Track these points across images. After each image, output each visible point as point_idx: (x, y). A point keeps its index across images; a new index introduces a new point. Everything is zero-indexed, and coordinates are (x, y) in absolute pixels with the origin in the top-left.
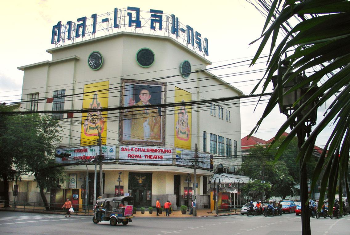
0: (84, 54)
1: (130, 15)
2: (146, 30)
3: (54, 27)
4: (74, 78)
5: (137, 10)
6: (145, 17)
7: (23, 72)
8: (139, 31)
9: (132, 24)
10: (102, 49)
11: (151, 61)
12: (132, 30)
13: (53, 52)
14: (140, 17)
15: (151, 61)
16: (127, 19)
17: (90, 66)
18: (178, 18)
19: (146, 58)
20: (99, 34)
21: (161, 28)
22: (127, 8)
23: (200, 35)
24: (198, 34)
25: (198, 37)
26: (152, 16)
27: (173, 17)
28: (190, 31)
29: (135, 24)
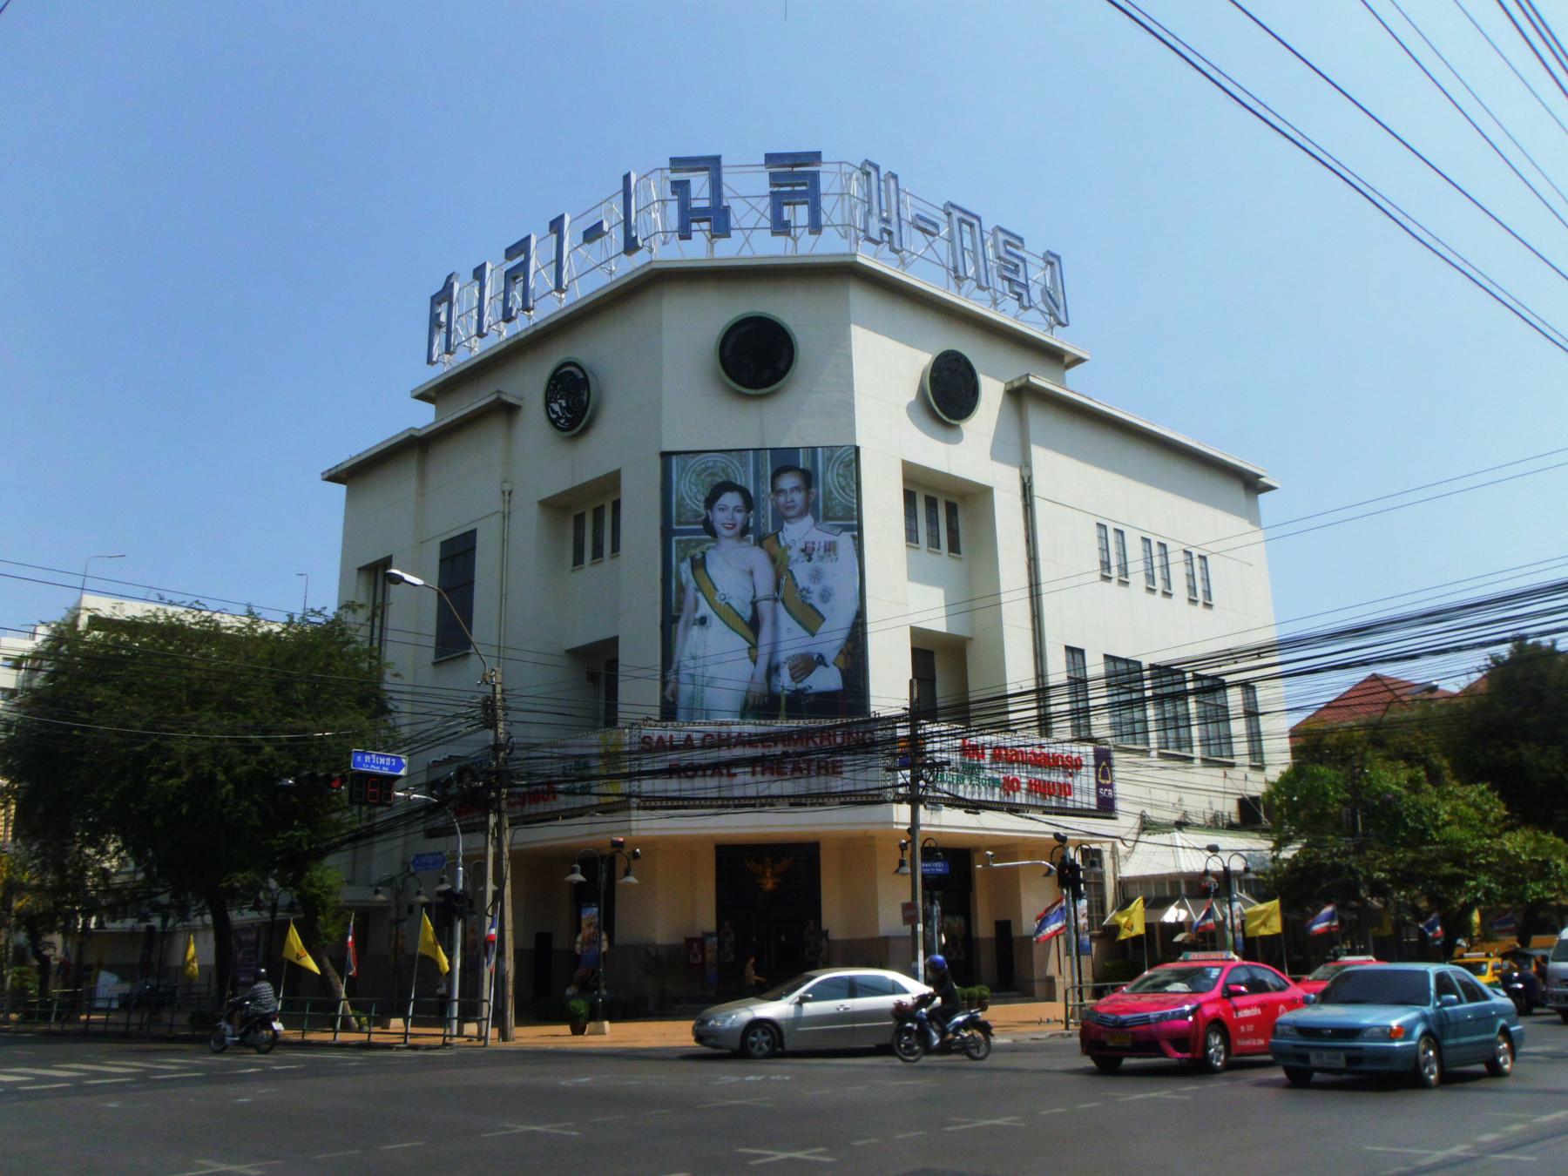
0: (528, 386)
1: (681, 188)
2: (752, 242)
3: (436, 300)
6: (748, 190)
7: (342, 489)
8: (728, 251)
10: (586, 350)
11: (782, 365)
12: (697, 250)
13: (432, 394)
14: (726, 192)
15: (782, 365)
17: (554, 422)
20: (580, 291)
21: (815, 227)
22: (667, 164)
26: (775, 179)
29: (705, 225)
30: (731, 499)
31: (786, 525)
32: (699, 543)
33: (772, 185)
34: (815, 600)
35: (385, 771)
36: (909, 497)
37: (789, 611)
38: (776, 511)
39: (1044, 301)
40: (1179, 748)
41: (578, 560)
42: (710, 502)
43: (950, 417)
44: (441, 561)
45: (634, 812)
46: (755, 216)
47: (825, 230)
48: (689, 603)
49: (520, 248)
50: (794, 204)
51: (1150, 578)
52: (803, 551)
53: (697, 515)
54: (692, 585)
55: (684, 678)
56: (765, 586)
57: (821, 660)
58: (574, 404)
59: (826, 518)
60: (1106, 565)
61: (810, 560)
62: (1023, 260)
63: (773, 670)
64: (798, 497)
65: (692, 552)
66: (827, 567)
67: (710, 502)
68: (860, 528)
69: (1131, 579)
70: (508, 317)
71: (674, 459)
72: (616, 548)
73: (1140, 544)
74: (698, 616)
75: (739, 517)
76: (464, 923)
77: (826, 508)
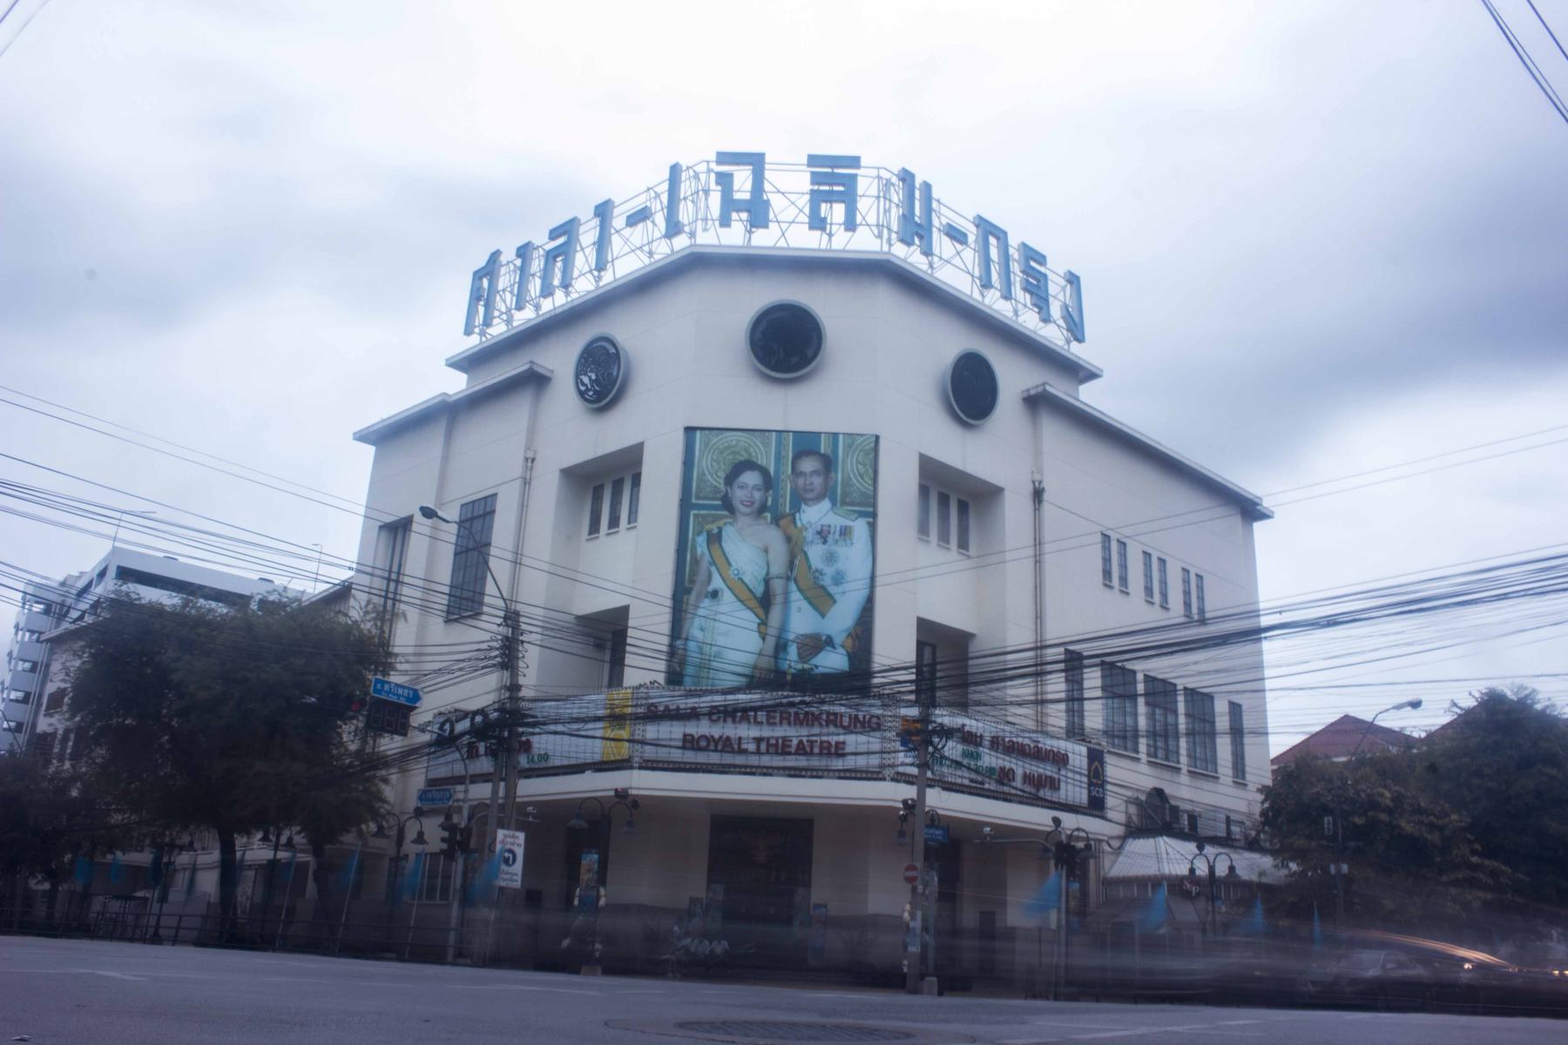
0: (560, 359)
1: (725, 180)
3: (478, 275)
4: (528, 448)
5: (756, 162)
6: (789, 188)
7: (371, 449)
8: (764, 240)
9: (734, 215)
12: (734, 237)
13: (469, 363)
14: (767, 187)
16: (715, 199)
17: (582, 394)
18: (927, 187)
19: (786, 345)
21: (850, 225)
22: (714, 158)
23: (1042, 259)
24: (1032, 256)
25: (1033, 264)
26: (816, 179)
27: (903, 180)
28: (992, 240)
29: (744, 216)
30: (750, 478)
31: (804, 507)
32: (716, 519)
33: (813, 183)
34: (827, 581)
35: (403, 701)
36: (924, 490)
37: (800, 590)
38: (794, 492)
39: (1063, 318)
40: (1167, 759)
41: (594, 528)
42: (730, 479)
43: (968, 416)
44: (456, 554)
45: (636, 772)
46: (793, 211)
47: (860, 229)
48: (701, 577)
49: (567, 230)
50: (831, 202)
51: (1149, 590)
52: (818, 533)
53: (716, 490)
54: (707, 558)
55: (692, 645)
56: (778, 567)
57: (829, 642)
58: (604, 379)
59: (844, 503)
60: (1107, 574)
61: (825, 542)
62: (1045, 276)
63: (781, 647)
64: (817, 481)
65: (708, 527)
66: (841, 550)
67: (730, 479)
68: (874, 515)
69: (1130, 590)
70: (547, 291)
71: (698, 433)
72: (633, 517)
73: (1141, 557)
74: (710, 588)
75: (757, 495)
76: (465, 860)
77: (844, 494)
